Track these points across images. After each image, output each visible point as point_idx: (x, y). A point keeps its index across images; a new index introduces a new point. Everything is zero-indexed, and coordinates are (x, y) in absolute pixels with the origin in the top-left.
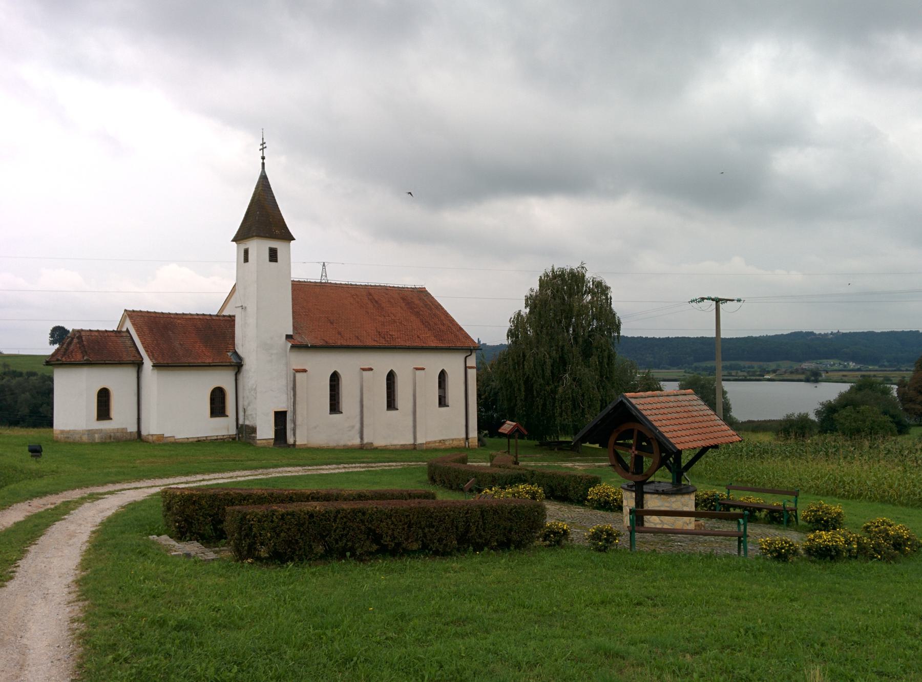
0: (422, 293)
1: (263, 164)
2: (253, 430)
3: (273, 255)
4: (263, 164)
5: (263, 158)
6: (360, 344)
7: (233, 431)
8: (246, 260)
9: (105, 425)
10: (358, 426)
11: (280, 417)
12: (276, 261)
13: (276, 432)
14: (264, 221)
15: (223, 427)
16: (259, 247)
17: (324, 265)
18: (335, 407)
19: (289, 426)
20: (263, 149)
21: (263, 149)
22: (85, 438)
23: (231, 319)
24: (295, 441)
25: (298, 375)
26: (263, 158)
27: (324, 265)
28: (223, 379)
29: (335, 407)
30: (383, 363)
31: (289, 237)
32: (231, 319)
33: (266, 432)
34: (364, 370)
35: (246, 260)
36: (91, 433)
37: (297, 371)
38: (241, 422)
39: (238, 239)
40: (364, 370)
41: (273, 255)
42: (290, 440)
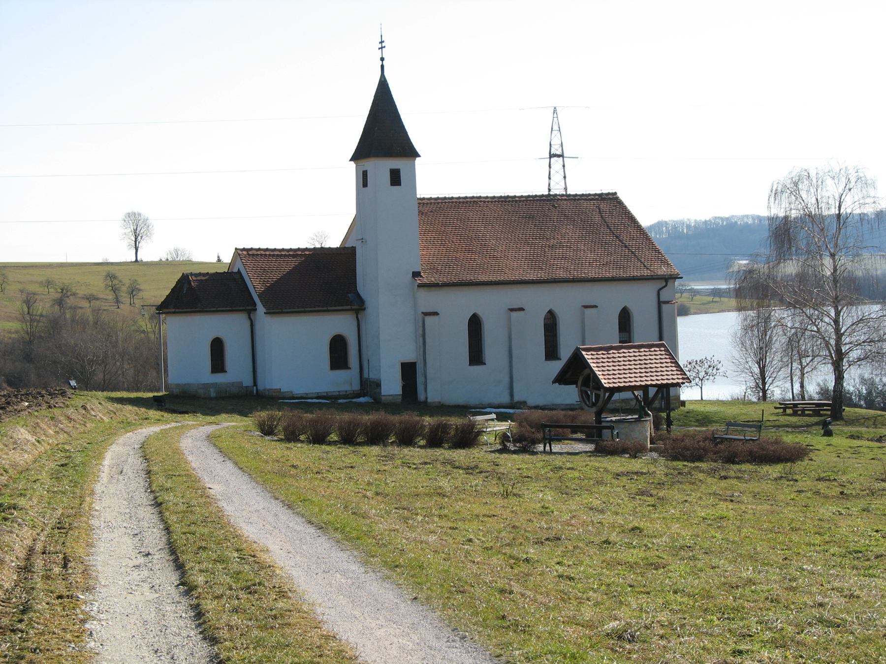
0: (612, 199)
1: (382, 66)
2: (378, 385)
3: (395, 178)
4: (382, 66)
5: (382, 59)
6: (646, 273)
7: (356, 387)
8: (365, 185)
9: (219, 378)
10: (506, 380)
11: (409, 371)
12: (400, 184)
13: (404, 388)
14: (384, 138)
15: (343, 381)
16: (381, 167)
17: (555, 111)
18: (476, 356)
19: (420, 379)
20: (382, 48)
21: (382, 48)
22: (201, 392)
23: (353, 249)
24: (427, 398)
25: (428, 319)
26: (382, 59)
27: (555, 111)
28: (340, 323)
29: (476, 356)
30: (538, 301)
31: (415, 154)
32: (353, 249)
33: (392, 385)
34: (512, 310)
35: (365, 185)
36: (206, 386)
37: (426, 314)
38: (366, 375)
39: (355, 158)
40: (512, 310)
41: (395, 178)
42: (421, 397)
